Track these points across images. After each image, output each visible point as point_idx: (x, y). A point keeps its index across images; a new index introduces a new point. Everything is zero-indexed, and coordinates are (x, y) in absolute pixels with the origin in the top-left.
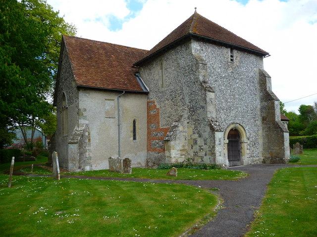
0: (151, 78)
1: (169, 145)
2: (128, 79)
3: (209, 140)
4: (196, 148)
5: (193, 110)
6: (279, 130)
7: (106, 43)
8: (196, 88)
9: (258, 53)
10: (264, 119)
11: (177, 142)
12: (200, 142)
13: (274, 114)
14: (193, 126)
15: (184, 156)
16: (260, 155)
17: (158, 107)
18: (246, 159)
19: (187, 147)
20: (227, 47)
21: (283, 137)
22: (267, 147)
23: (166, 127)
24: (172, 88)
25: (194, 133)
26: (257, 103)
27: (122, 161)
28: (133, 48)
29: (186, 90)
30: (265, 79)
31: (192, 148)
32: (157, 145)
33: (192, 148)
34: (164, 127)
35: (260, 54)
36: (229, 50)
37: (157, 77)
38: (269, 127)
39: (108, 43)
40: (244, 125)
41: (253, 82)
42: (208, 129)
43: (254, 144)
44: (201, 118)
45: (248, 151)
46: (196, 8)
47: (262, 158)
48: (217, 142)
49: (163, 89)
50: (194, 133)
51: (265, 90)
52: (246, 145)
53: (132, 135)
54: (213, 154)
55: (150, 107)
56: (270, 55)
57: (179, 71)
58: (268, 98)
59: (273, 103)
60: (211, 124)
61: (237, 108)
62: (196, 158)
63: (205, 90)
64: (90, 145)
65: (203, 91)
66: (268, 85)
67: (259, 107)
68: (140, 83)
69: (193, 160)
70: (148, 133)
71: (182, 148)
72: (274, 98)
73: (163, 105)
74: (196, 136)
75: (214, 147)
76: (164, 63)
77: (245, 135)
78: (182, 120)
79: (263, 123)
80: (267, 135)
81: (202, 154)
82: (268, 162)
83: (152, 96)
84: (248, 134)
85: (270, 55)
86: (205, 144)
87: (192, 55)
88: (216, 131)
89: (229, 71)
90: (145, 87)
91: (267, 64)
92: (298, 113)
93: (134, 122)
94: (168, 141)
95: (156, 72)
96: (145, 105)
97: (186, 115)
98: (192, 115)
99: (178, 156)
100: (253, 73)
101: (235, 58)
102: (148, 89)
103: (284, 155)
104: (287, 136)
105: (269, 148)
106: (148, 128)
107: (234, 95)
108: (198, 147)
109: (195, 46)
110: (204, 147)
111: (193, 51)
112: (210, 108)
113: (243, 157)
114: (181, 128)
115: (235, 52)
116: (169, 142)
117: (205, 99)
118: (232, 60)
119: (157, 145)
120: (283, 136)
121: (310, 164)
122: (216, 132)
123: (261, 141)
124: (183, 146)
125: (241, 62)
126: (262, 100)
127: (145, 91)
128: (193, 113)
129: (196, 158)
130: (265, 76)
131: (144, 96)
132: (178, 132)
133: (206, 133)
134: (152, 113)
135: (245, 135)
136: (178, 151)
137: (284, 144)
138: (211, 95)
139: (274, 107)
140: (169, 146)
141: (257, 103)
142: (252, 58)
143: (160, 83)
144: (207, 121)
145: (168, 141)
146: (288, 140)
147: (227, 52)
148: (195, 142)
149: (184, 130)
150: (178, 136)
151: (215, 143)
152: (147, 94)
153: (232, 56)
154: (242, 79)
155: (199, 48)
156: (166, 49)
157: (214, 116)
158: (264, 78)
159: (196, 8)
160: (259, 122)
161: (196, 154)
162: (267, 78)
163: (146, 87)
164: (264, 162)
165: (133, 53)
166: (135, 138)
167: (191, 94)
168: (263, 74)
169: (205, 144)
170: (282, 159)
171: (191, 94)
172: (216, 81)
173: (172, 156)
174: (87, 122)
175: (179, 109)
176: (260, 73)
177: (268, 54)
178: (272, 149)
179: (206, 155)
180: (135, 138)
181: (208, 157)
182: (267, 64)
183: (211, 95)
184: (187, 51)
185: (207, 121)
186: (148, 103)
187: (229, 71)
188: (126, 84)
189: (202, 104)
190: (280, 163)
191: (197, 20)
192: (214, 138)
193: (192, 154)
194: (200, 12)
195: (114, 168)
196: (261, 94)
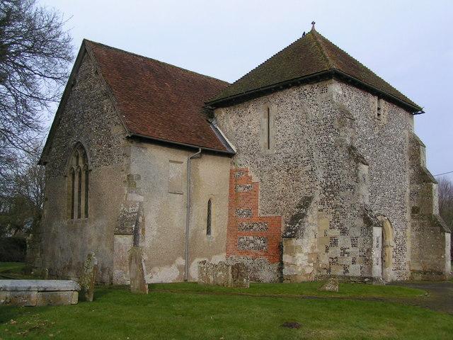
0: (228, 124)
4: (334, 252)
6: (438, 228)
7: (151, 60)
8: (341, 155)
9: (409, 107)
10: (415, 210)
11: (305, 240)
12: (344, 241)
13: (431, 205)
14: (331, 217)
20: (374, 95)
21: (443, 239)
23: (274, 215)
24: (291, 150)
25: (332, 228)
32: (252, 245)
34: (268, 215)
35: (412, 109)
36: (376, 98)
39: (154, 60)
41: (402, 152)
46: (313, 23)
48: (375, 244)
49: (269, 152)
51: (418, 165)
53: (206, 226)
54: (367, 261)
55: (235, 179)
56: (423, 112)
57: (307, 125)
58: (423, 177)
59: (431, 188)
60: (365, 215)
64: (144, 239)
65: (352, 162)
66: (422, 158)
68: (216, 134)
69: (329, 271)
74: (336, 232)
75: (369, 250)
80: (418, 236)
83: (241, 161)
85: (423, 112)
86: (354, 245)
87: (333, 103)
88: (375, 226)
91: (420, 125)
96: (227, 175)
98: (328, 198)
101: (382, 112)
102: (233, 147)
103: (444, 267)
105: (421, 256)
107: (380, 171)
108: (338, 250)
109: (336, 88)
110: (351, 250)
112: (364, 190)
114: (310, 219)
115: (383, 102)
117: (357, 175)
119: (252, 245)
120: (444, 237)
122: (374, 228)
123: (408, 245)
127: (230, 151)
128: (332, 195)
131: (226, 159)
132: (306, 224)
136: (305, 254)
139: (432, 194)
142: (402, 113)
143: (263, 141)
148: (334, 242)
151: (371, 244)
152: (230, 155)
155: (340, 92)
156: (281, 87)
157: (367, 202)
158: (416, 147)
159: (313, 23)
160: (408, 216)
167: (329, 165)
169: (354, 245)
174: (141, 198)
177: (421, 109)
179: (354, 262)
182: (420, 125)
183: (364, 169)
186: (232, 172)
189: (350, 181)
194: (318, 29)
195: (211, 278)
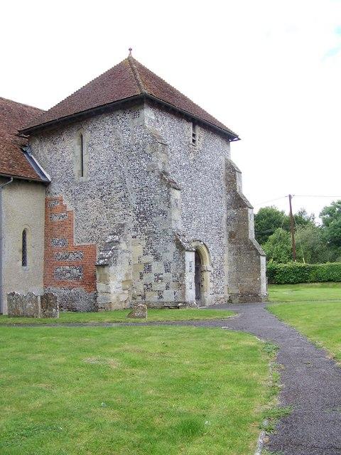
1: (106, 272)
2: (13, 157)
3: (173, 266)
4: (149, 278)
5: (144, 216)
8: (152, 180)
11: (119, 267)
12: (157, 267)
14: (144, 243)
15: (126, 292)
16: (226, 290)
17: (70, 208)
18: (209, 297)
19: (131, 277)
20: (188, 121)
21: (259, 261)
22: (236, 281)
25: (145, 254)
26: (223, 212)
27: (39, 298)
28: (7, 100)
29: (131, 184)
30: (235, 175)
31: (141, 278)
33: (141, 278)
34: (83, 244)
35: (228, 136)
36: (190, 125)
37: (70, 157)
38: (239, 248)
40: (207, 244)
42: (172, 247)
43: (219, 273)
44: (159, 229)
45: (211, 285)
46: (130, 50)
47: (228, 296)
49: (83, 179)
50: (145, 254)
51: (235, 191)
52: (209, 274)
53: (21, 258)
55: (49, 208)
56: (239, 139)
58: (239, 202)
59: (246, 212)
61: (200, 217)
62: (148, 294)
63: (169, 186)
67: (225, 216)
69: (144, 297)
70: (46, 254)
71: (124, 279)
72: (247, 203)
73: (80, 205)
74: (150, 258)
75: (182, 275)
76: (87, 136)
77: (208, 259)
78: (125, 233)
79: (230, 241)
80: (236, 260)
81: (160, 286)
82: (236, 300)
84: (212, 258)
85: (239, 139)
86: (167, 271)
88: (187, 251)
89: (192, 157)
90: (41, 172)
91: (236, 153)
92: (319, 222)
93: (24, 233)
94: (103, 266)
95: (69, 148)
97: (131, 222)
99: (120, 290)
100: (219, 164)
101: (197, 138)
104: (263, 259)
106: (46, 245)
109: (148, 114)
111: (146, 122)
112: (176, 215)
113: (205, 294)
114: (123, 246)
115: (198, 128)
116: (106, 268)
117: (168, 200)
118: (194, 141)
119: (69, 275)
121: (160, 323)
122: (186, 252)
123: (226, 269)
124: (127, 275)
125: (205, 145)
126: (229, 206)
127: (43, 179)
128: (145, 221)
129: (148, 294)
130: (235, 171)
132: (119, 251)
133: (170, 252)
134: (56, 219)
135: (208, 259)
137: (260, 273)
138: (176, 194)
139: (247, 218)
140: (106, 274)
141: (222, 211)
142: (218, 141)
143: (77, 168)
144: (170, 234)
145: (103, 266)
146: (265, 269)
147: (188, 127)
148: (148, 268)
149: (131, 250)
150: (120, 258)
152: (45, 185)
153: (194, 135)
154: (205, 173)
155: (153, 118)
158: (232, 174)
159: (130, 50)
160: (225, 241)
161: (148, 287)
162: (237, 173)
163: (45, 173)
164: (230, 301)
165: (9, 110)
166: (24, 264)
167: (142, 190)
168: (232, 167)
169: (167, 271)
170: (256, 295)
171: (142, 190)
172: (174, 172)
173: (112, 291)
175: (117, 214)
176: (226, 165)
177: (237, 136)
178: (243, 282)
179: (167, 288)
180: (24, 264)
181: (171, 291)
182: (236, 153)
183: (176, 194)
184: (136, 121)
185: (170, 234)
187: (192, 157)
188: (10, 166)
189: (162, 207)
190: (253, 301)
191: (128, 70)
192: (184, 262)
193: (141, 288)
196: (229, 197)
